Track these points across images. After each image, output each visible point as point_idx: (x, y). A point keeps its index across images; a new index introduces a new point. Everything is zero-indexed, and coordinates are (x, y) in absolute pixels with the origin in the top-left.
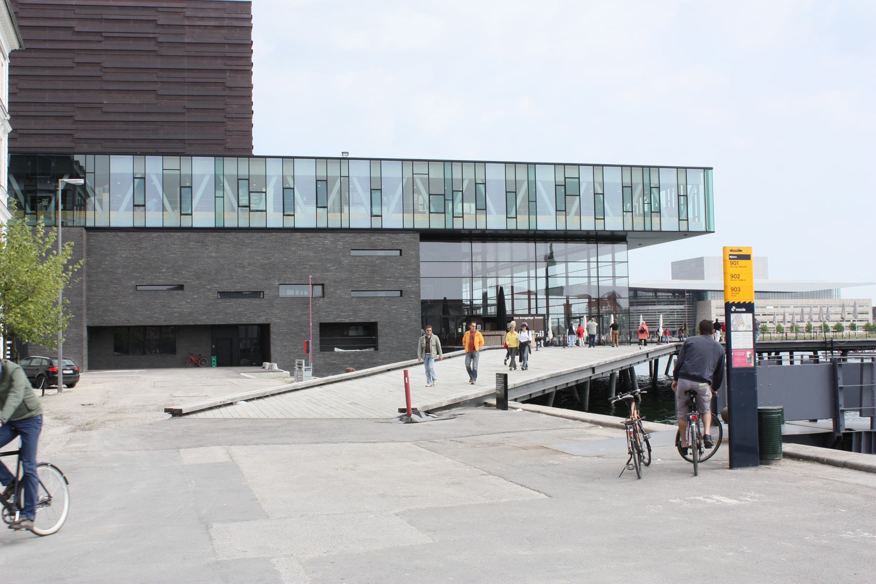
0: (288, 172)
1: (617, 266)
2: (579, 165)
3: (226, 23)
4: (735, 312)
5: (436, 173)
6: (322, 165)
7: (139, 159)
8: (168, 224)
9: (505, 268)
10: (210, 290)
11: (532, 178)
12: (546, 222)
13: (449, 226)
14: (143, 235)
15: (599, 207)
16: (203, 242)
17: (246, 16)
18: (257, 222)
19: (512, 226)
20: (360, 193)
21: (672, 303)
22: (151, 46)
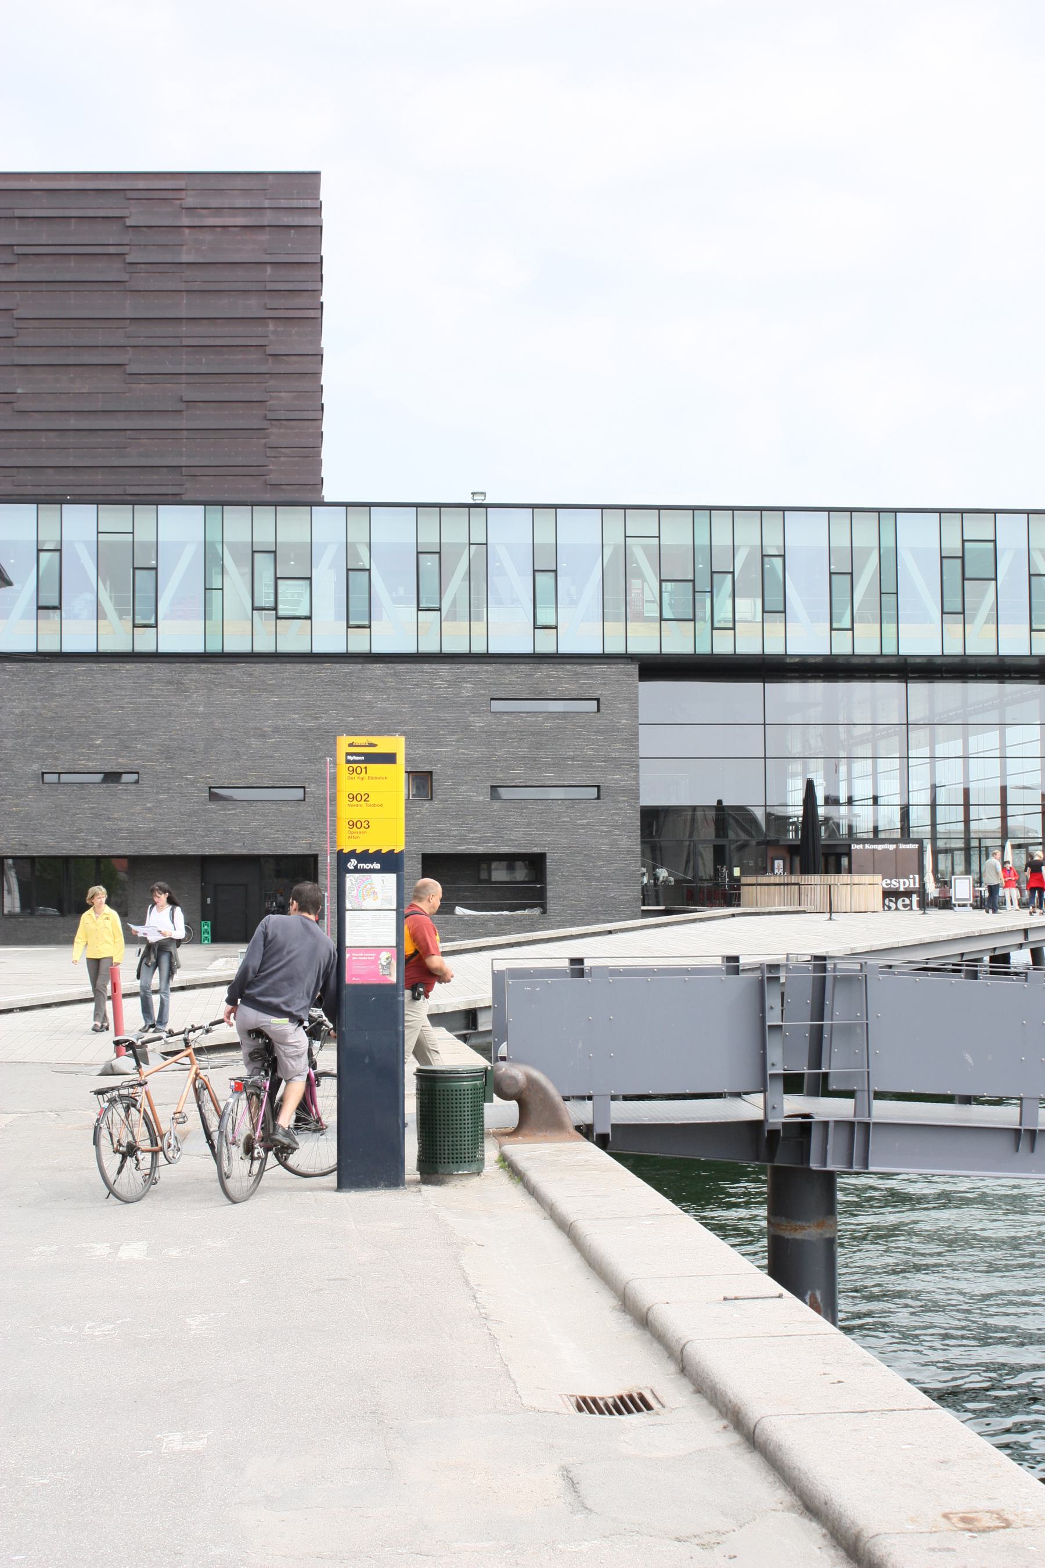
0: (358, 535)
2: (995, 512)
3: (268, 219)
4: (356, 870)
5: (677, 533)
7: (49, 511)
8: (108, 646)
10: (192, 783)
11: (888, 541)
12: (920, 640)
13: (703, 649)
14: (57, 668)
16: (179, 683)
17: (309, 203)
18: (292, 640)
19: (842, 646)
20: (511, 580)
22: (113, 272)
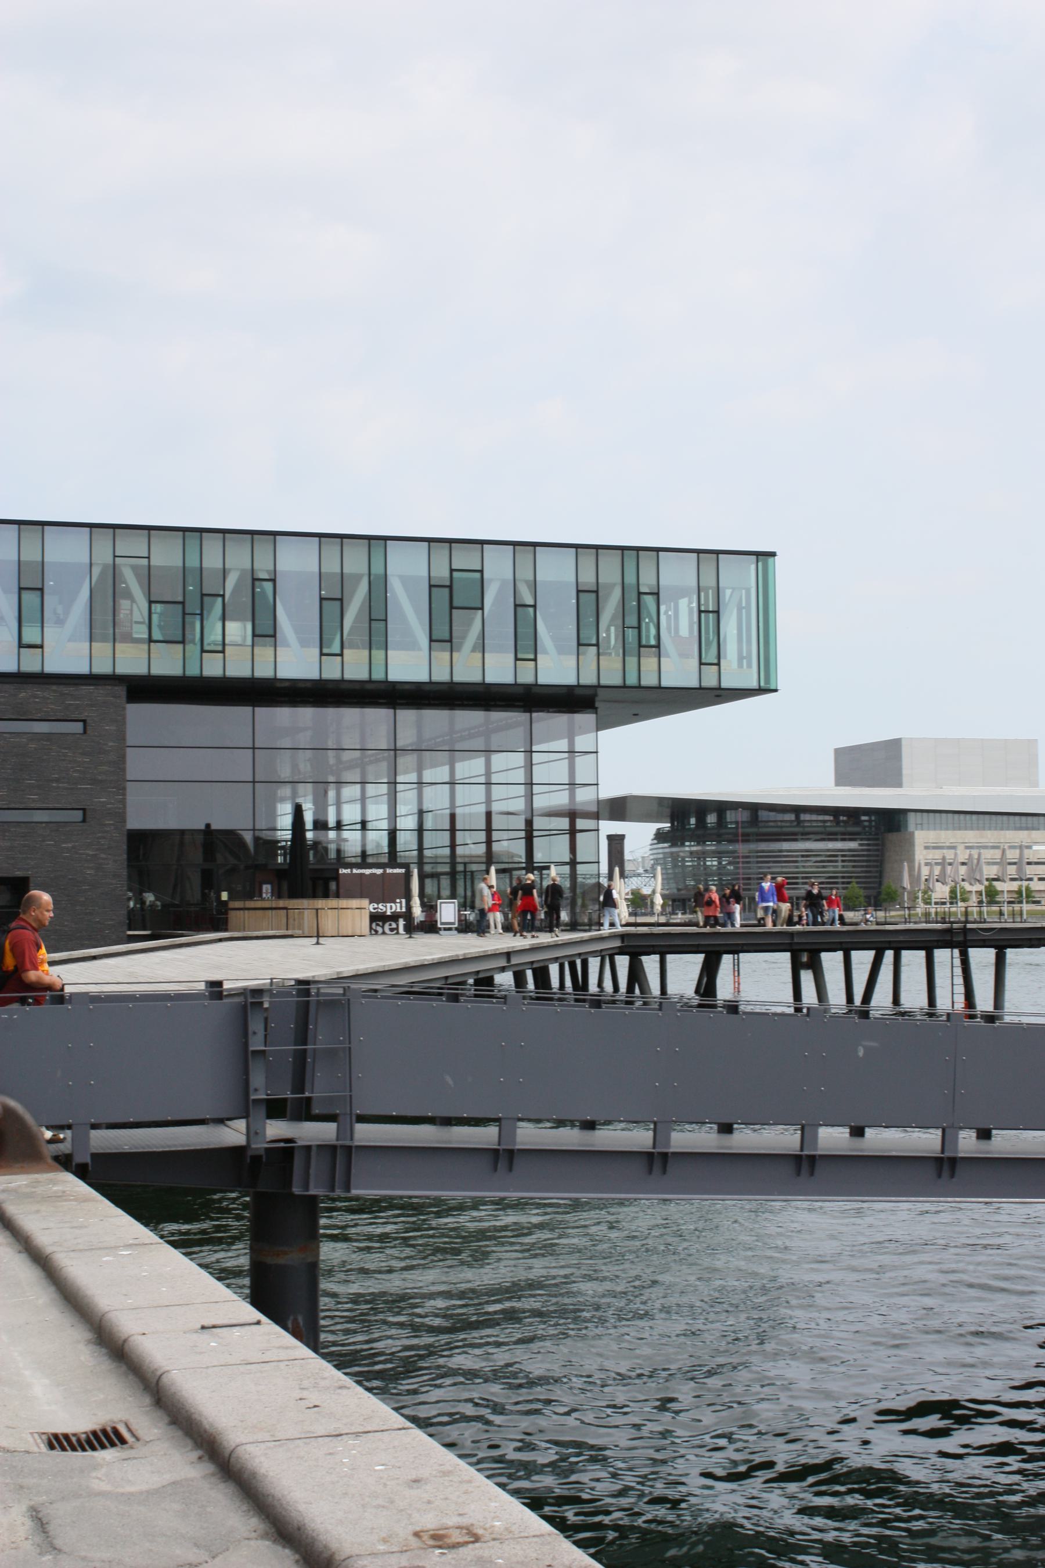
1: (579, 760)
6: (332, 549)
9: (377, 761)
12: (408, 664)
13: (193, 671)
15: (525, 630)
19: (332, 671)
21: (831, 836)
